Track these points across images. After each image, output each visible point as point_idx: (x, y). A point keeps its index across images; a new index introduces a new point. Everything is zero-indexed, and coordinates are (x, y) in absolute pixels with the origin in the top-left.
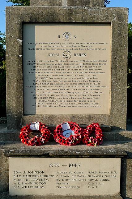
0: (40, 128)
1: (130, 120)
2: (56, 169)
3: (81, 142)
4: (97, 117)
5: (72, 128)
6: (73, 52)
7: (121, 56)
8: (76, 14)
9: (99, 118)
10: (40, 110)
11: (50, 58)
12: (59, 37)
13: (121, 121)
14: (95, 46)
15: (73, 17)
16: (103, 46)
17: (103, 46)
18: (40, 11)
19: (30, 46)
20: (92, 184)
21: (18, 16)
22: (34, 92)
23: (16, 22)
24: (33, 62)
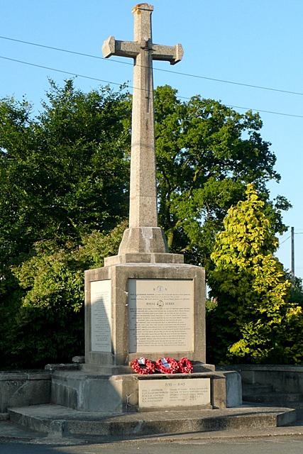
0: (146, 362)
1: (80, 328)
2: (170, 387)
3: (179, 371)
4: (184, 354)
5: (169, 362)
6: (165, 301)
7: (200, 305)
8: (168, 272)
9: (186, 354)
10: (140, 350)
11: (149, 306)
12: (154, 289)
13: (202, 357)
14: (183, 297)
15: (166, 274)
16: (187, 297)
17: (187, 297)
18: (142, 270)
19: (132, 297)
20: (192, 397)
21: (125, 273)
22: (135, 334)
23: (123, 277)
24: (134, 310)
